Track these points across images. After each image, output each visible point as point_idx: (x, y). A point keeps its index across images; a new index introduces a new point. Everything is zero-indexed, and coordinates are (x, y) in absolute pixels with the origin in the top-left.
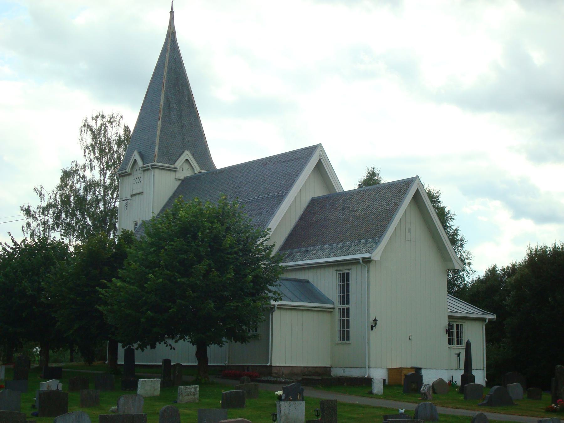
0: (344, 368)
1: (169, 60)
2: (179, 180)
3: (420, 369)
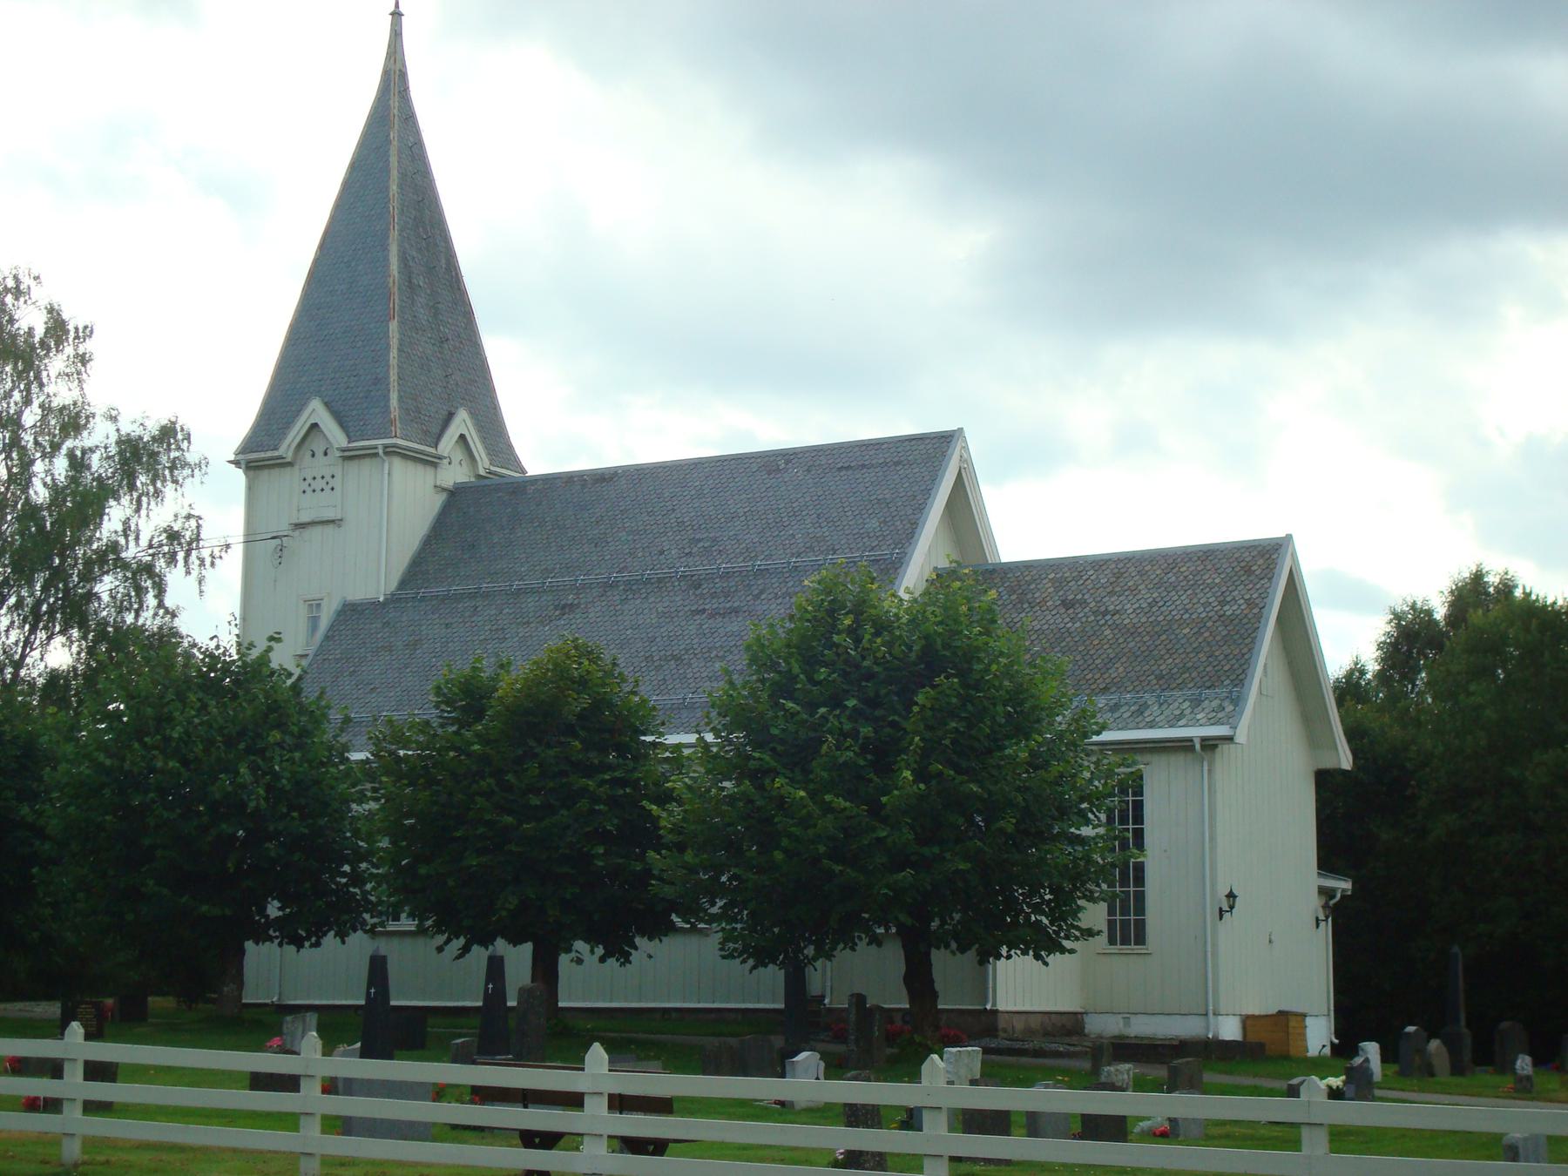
0: (1128, 1015)
1: (400, 152)
2: (444, 489)
3: (1304, 1015)
